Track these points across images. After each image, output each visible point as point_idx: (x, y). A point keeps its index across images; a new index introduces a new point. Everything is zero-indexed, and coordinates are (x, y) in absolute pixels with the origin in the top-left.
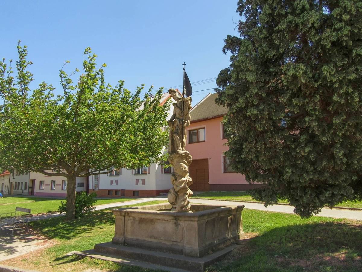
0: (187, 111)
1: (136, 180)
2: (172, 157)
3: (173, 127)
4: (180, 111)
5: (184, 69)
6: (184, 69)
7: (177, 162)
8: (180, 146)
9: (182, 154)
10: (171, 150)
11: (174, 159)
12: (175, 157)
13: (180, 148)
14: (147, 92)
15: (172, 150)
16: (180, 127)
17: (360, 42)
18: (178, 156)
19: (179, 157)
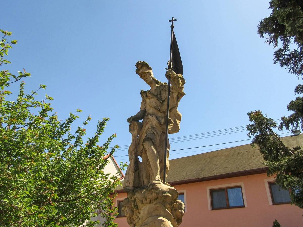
0: (174, 101)
1: (141, 91)
2: (135, 201)
3: (138, 134)
4: (158, 102)
5: (172, 27)
6: (172, 27)
7: (150, 214)
8: (157, 174)
9: (165, 192)
10: (131, 184)
11: (140, 205)
12: (145, 198)
13: (158, 177)
14: (81, 125)
15: (134, 182)
16: (159, 131)
17: (183, 195)
18: (154, 195)
19: (156, 199)
